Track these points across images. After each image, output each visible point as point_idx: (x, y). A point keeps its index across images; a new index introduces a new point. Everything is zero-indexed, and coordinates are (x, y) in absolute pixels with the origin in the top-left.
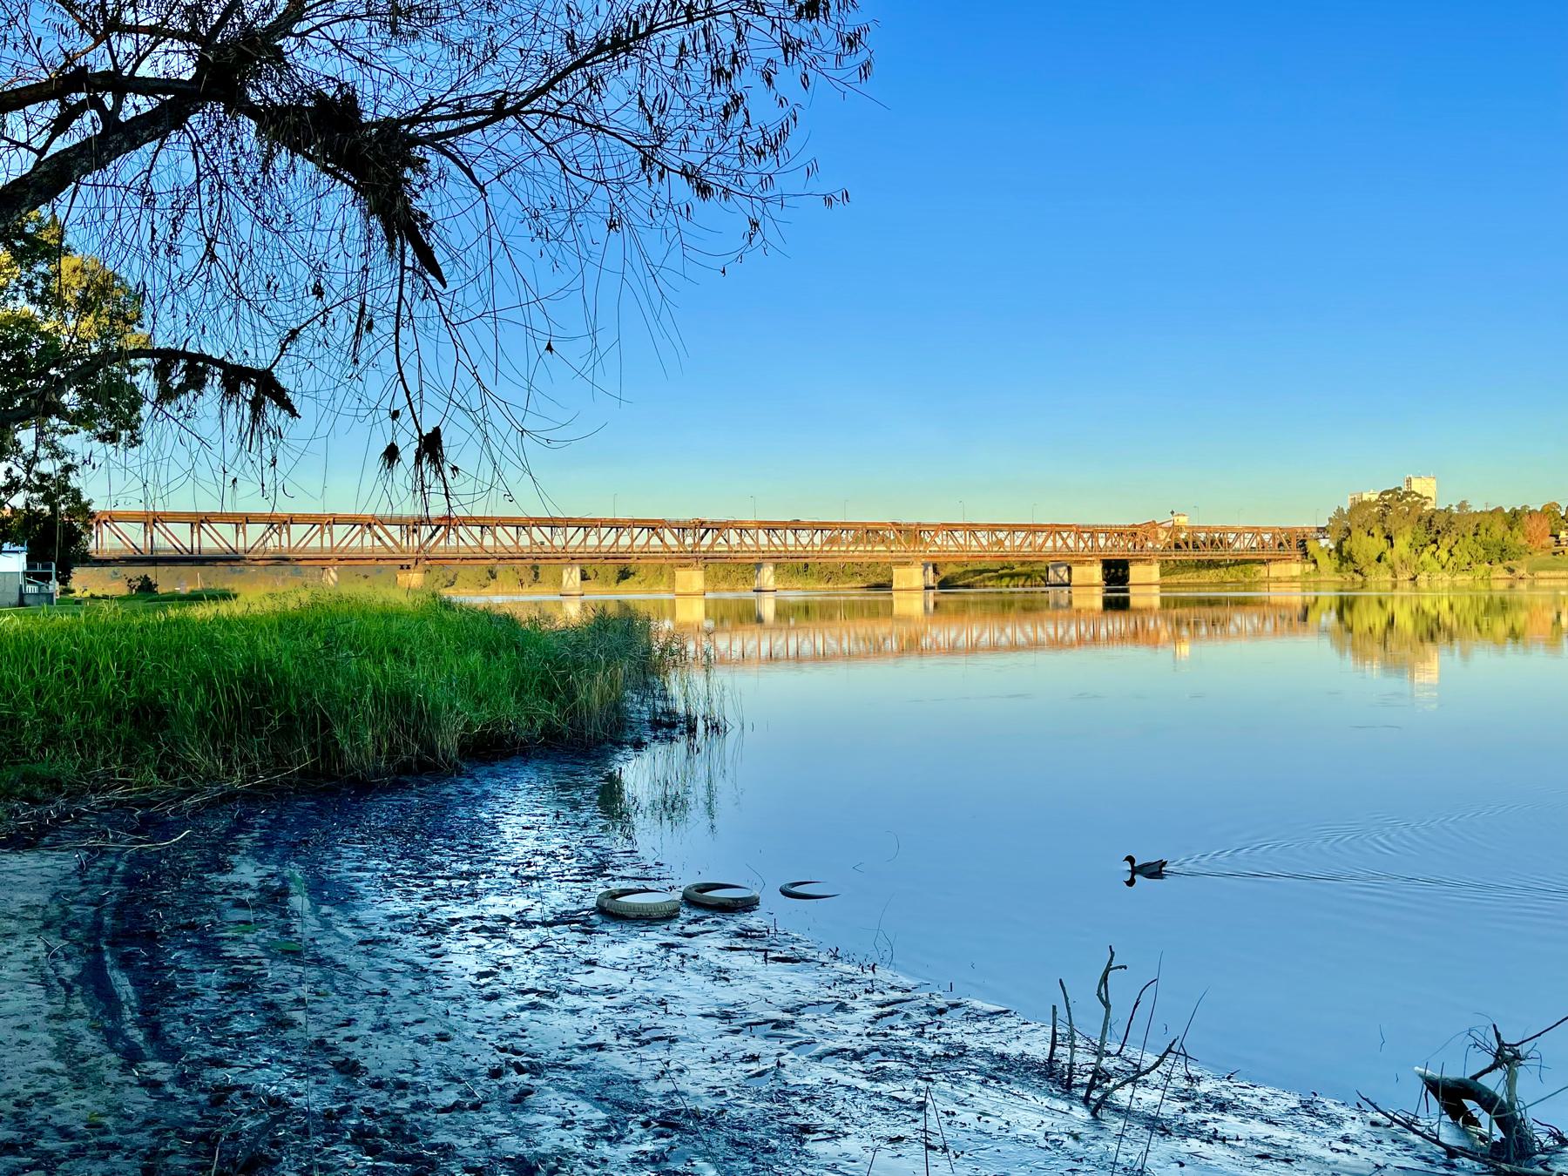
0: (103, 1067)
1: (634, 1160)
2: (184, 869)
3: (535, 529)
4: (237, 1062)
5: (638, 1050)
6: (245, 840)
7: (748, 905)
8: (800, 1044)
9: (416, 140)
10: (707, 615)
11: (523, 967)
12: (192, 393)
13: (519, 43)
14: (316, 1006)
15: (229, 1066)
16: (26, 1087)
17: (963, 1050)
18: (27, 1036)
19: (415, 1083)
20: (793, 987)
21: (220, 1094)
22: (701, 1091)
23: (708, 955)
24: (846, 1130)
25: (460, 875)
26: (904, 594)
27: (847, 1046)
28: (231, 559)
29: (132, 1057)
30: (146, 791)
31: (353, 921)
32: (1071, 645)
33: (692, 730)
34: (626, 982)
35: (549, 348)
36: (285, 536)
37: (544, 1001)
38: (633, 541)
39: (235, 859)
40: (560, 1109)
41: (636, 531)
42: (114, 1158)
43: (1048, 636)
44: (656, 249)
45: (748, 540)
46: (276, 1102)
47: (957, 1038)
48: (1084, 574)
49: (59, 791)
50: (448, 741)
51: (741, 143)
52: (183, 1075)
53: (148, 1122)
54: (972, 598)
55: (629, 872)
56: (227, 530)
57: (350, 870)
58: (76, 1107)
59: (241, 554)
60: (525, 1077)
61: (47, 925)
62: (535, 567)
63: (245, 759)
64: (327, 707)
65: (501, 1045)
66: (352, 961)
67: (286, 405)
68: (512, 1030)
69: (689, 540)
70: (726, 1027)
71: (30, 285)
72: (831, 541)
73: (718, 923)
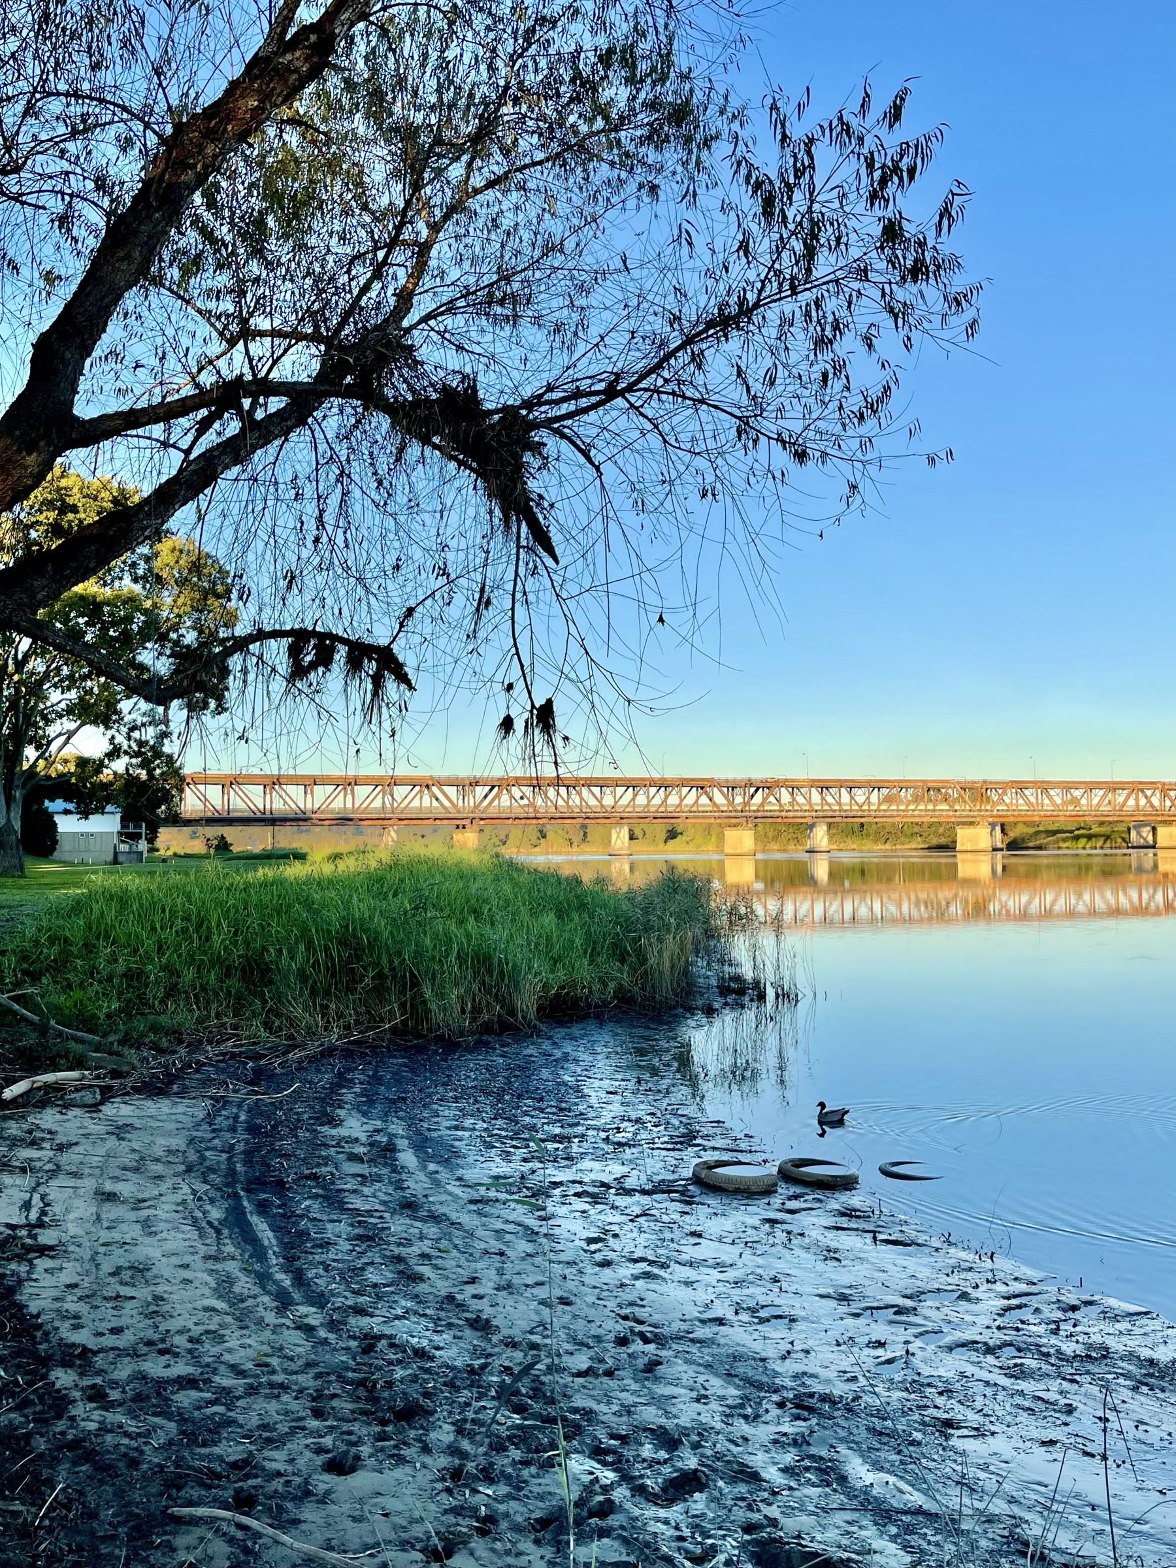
0: (261, 1309)
1: (775, 1442)
2: (298, 1120)
4: (377, 1312)
5: (759, 1327)
6: (348, 1095)
7: (847, 1184)
8: (927, 1332)
9: (535, 425)
10: (757, 876)
11: (630, 1235)
12: (321, 670)
13: (626, 325)
14: (439, 1262)
15: (372, 1316)
16: (196, 1324)
17: (1105, 1353)
18: (187, 1274)
19: (546, 1345)
20: (910, 1272)
21: (369, 1342)
22: (832, 1375)
23: (815, 1234)
24: (993, 1428)
25: (555, 1138)
26: (969, 856)
27: (978, 1338)
28: (299, 819)
29: (284, 1302)
30: (254, 1044)
31: (460, 1179)
32: (1157, 913)
33: (762, 997)
34: (736, 1257)
35: (661, 620)
36: (349, 797)
37: (656, 1271)
38: (682, 800)
39: (342, 1113)
40: (691, 1382)
42: (285, 1398)
43: (1131, 903)
44: (756, 516)
45: (800, 799)
46: (420, 1354)
47: (1096, 1339)
48: (1171, 835)
49: (180, 1042)
50: (527, 1001)
51: (841, 408)
52: (332, 1321)
53: (309, 1365)
54: (1045, 861)
55: (719, 1142)
56: (296, 791)
57: (449, 1128)
58: (243, 1346)
59: (309, 814)
60: (651, 1348)
61: (189, 1170)
62: (584, 826)
63: (340, 1016)
64: (416, 965)
65: (623, 1312)
66: (467, 1219)
67: (403, 678)
68: (630, 1298)
69: (739, 799)
70: (845, 1309)
71: (134, 565)
72: (889, 799)
73: (819, 1200)
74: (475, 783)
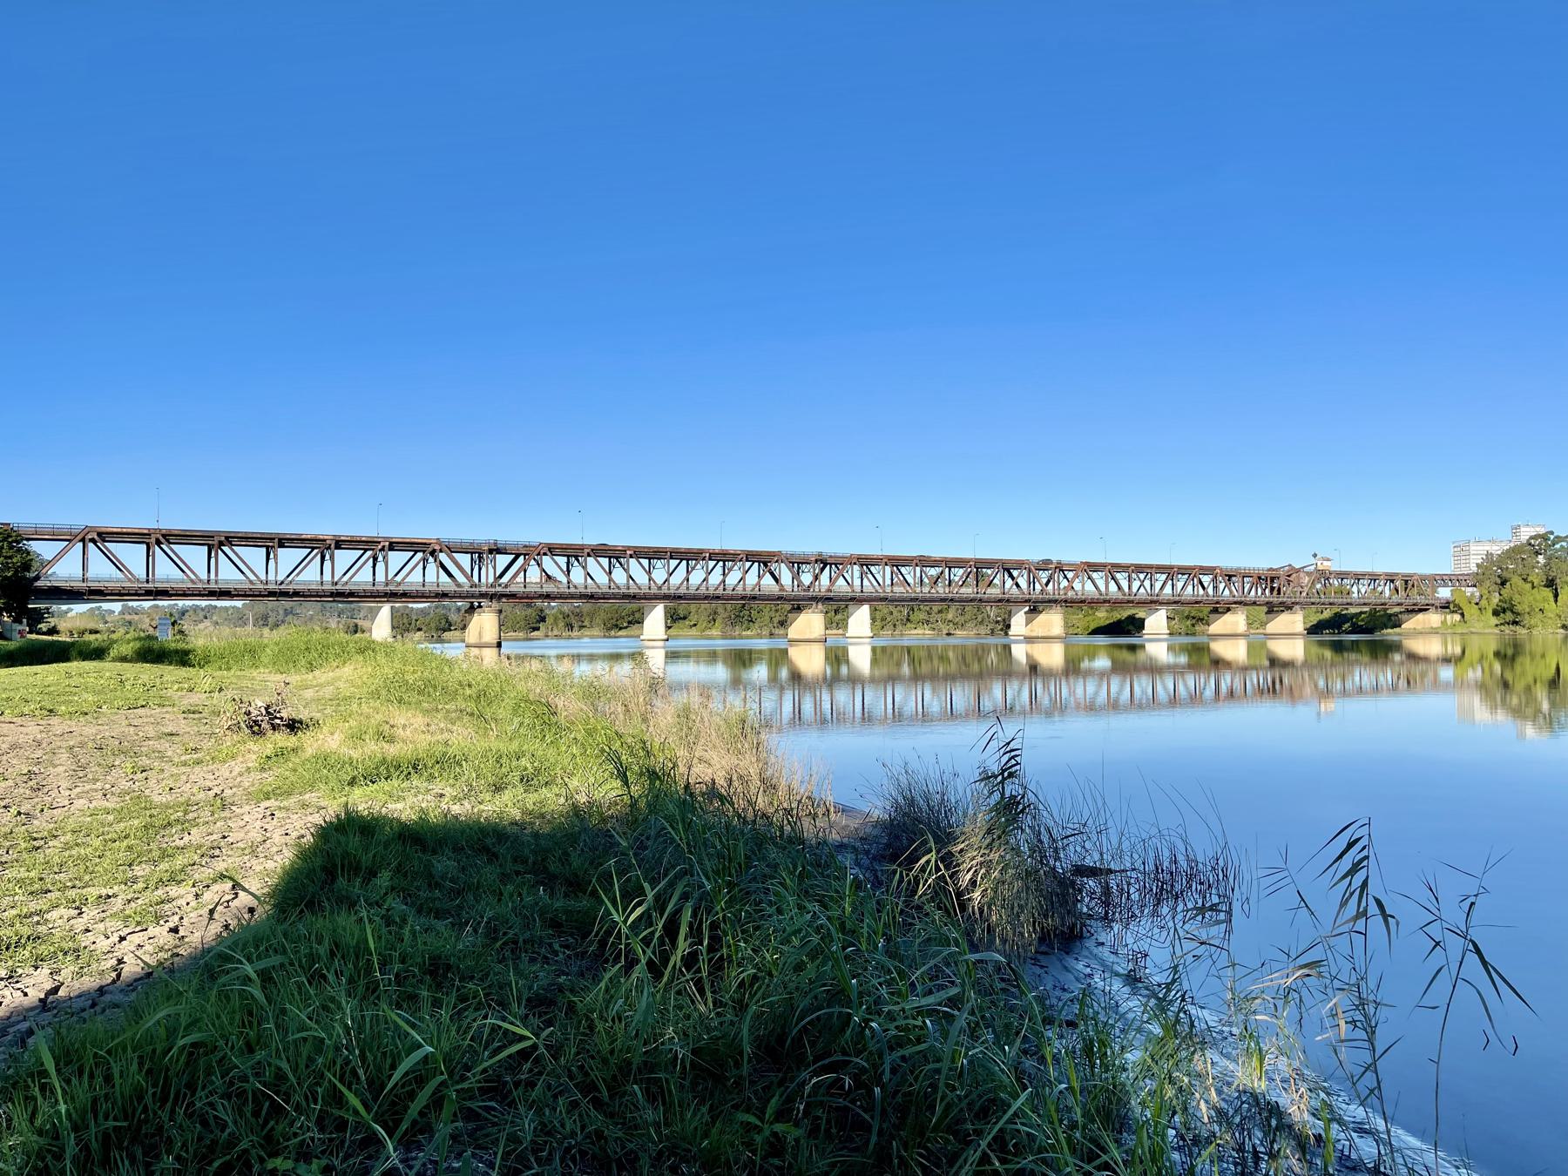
3: (633, 561)
41: (674, 563)
56: (195, 556)
74: (497, 550)
